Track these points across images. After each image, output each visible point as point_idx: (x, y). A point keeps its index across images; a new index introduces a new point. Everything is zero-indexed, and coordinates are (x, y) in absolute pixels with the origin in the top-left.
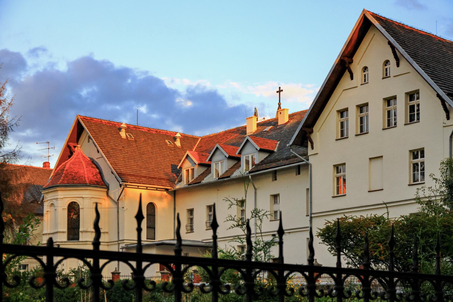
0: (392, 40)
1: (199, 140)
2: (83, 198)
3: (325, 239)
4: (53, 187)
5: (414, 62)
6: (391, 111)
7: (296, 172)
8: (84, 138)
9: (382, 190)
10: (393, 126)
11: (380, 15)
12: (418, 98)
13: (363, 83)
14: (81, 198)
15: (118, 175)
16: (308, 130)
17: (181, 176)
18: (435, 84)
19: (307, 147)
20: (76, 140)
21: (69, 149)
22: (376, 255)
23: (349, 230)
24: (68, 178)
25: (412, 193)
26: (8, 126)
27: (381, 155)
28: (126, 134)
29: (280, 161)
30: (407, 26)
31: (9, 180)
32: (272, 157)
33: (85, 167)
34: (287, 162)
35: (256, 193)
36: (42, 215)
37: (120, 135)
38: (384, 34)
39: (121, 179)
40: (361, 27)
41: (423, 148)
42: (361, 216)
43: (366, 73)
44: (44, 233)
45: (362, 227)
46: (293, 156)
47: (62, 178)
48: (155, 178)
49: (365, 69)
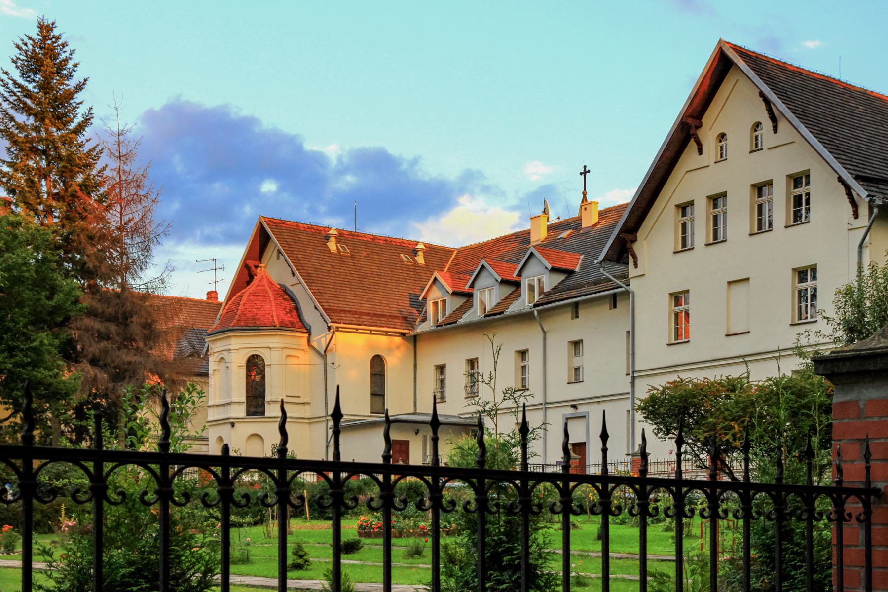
0: (766, 90)
1: (455, 254)
3: (648, 415)
4: (223, 332)
5: (802, 125)
6: (718, 216)
7: (610, 304)
8: (270, 253)
9: (749, 332)
10: (767, 229)
11: (746, 48)
12: (808, 184)
13: (719, 159)
14: (268, 349)
16: (628, 237)
18: (835, 160)
19: (627, 264)
20: (258, 256)
21: (246, 271)
22: (727, 440)
23: (686, 400)
25: (788, 338)
26: (152, 236)
27: (747, 277)
29: (584, 287)
30: (791, 65)
31: (154, 321)
33: (272, 299)
34: (596, 288)
35: (545, 339)
36: (206, 375)
37: (328, 247)
38: (753, 80)
40: (715, 69)
41: (816, 265)
42: (705, 379)
44: (209, 404)
45: (705, 396)
46: (604, 279)
47: (234, 321)
48: (384, 316)
49: (722, 136)
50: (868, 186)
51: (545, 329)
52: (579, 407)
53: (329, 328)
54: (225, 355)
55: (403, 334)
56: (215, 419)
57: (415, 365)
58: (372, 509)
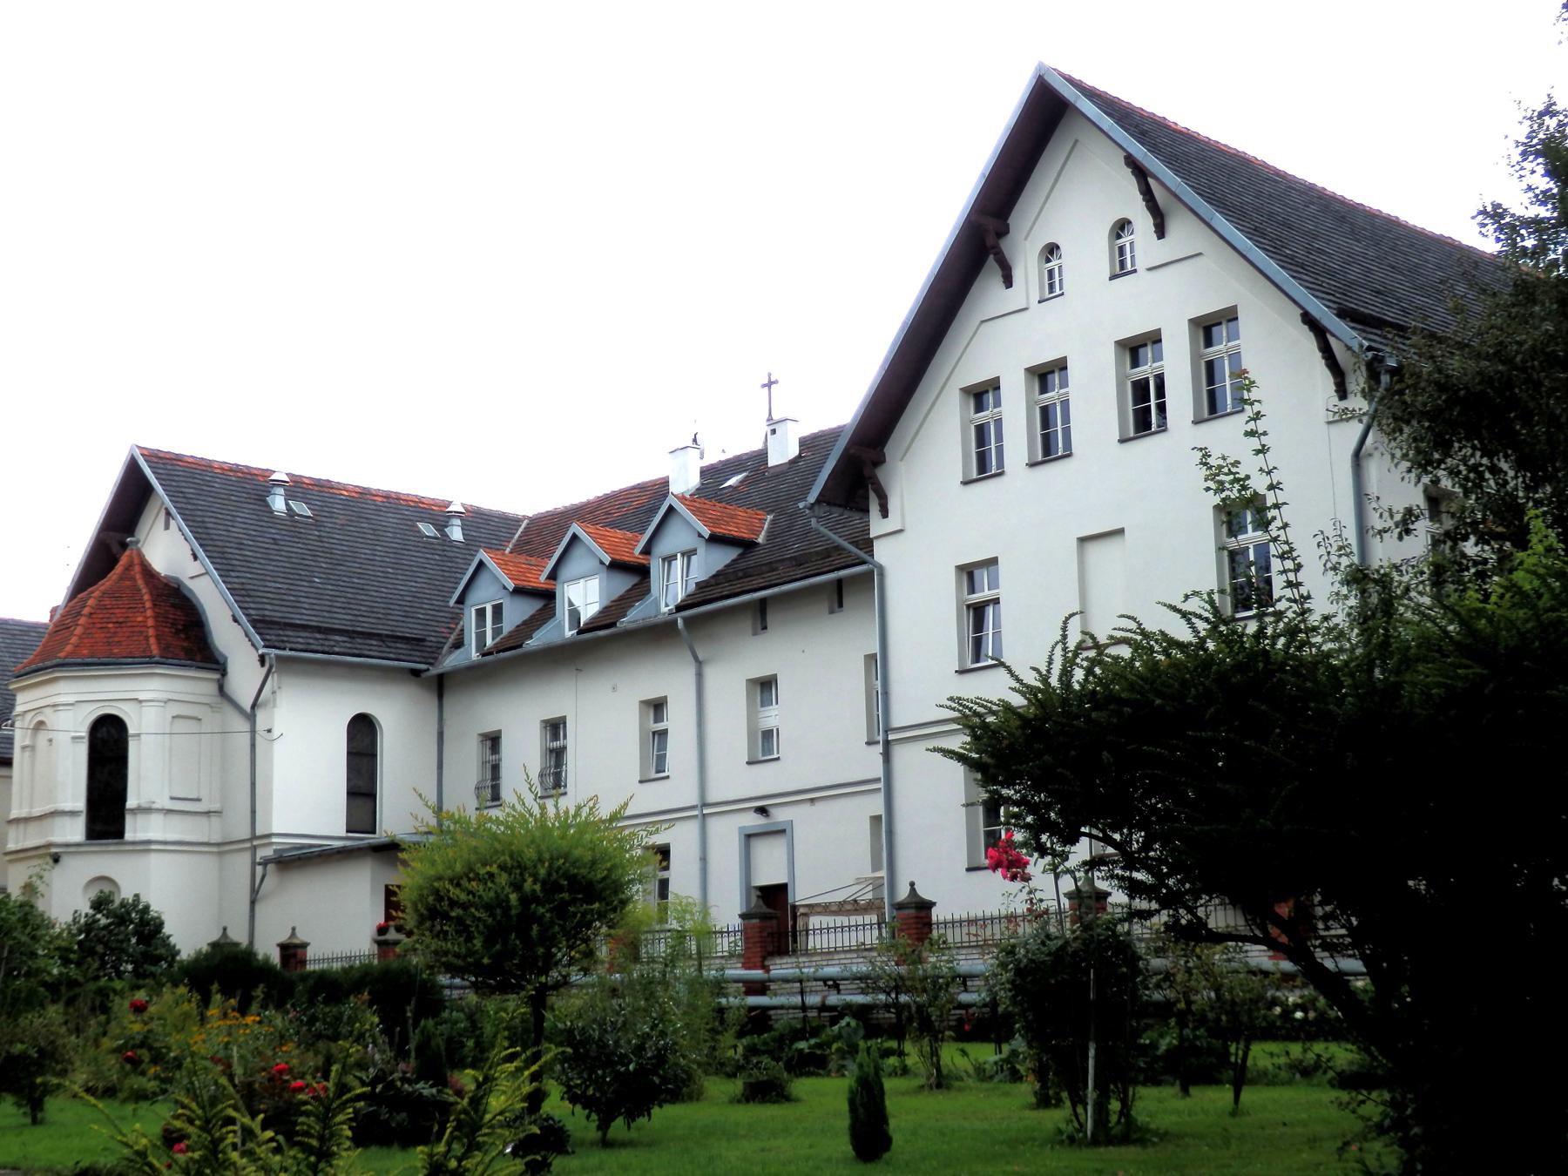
0: (1139, 151)
2: (141, 702)
15: (254, 627)
17: (462, 630)
19: (866, 511)
24: (93, 640)
28: (287, 504)
32: (755, 558)
33: (148, 605)
35: (700, 676)
37: (268, 506)
39: (263, 640)
43: (1054, 263)
44: (14, 814)
47: (74, 640)
49: (1052, 250)
50: (1364, 331)
51: (701, 657)
52: (773, 811)
53: (262, 659)
54: (48, 716)
55: (416, 673)
56: (19, 847)
57: (441, 735)
58: (1031, 856)
